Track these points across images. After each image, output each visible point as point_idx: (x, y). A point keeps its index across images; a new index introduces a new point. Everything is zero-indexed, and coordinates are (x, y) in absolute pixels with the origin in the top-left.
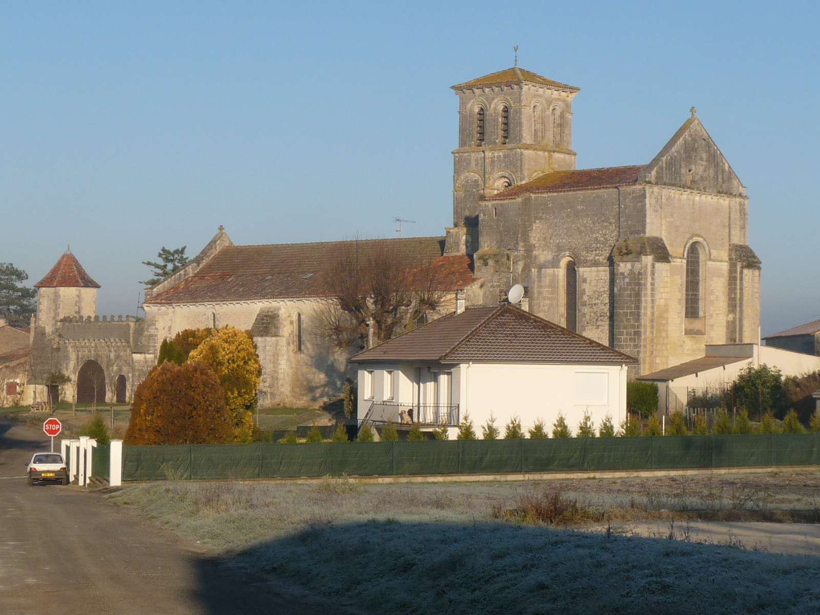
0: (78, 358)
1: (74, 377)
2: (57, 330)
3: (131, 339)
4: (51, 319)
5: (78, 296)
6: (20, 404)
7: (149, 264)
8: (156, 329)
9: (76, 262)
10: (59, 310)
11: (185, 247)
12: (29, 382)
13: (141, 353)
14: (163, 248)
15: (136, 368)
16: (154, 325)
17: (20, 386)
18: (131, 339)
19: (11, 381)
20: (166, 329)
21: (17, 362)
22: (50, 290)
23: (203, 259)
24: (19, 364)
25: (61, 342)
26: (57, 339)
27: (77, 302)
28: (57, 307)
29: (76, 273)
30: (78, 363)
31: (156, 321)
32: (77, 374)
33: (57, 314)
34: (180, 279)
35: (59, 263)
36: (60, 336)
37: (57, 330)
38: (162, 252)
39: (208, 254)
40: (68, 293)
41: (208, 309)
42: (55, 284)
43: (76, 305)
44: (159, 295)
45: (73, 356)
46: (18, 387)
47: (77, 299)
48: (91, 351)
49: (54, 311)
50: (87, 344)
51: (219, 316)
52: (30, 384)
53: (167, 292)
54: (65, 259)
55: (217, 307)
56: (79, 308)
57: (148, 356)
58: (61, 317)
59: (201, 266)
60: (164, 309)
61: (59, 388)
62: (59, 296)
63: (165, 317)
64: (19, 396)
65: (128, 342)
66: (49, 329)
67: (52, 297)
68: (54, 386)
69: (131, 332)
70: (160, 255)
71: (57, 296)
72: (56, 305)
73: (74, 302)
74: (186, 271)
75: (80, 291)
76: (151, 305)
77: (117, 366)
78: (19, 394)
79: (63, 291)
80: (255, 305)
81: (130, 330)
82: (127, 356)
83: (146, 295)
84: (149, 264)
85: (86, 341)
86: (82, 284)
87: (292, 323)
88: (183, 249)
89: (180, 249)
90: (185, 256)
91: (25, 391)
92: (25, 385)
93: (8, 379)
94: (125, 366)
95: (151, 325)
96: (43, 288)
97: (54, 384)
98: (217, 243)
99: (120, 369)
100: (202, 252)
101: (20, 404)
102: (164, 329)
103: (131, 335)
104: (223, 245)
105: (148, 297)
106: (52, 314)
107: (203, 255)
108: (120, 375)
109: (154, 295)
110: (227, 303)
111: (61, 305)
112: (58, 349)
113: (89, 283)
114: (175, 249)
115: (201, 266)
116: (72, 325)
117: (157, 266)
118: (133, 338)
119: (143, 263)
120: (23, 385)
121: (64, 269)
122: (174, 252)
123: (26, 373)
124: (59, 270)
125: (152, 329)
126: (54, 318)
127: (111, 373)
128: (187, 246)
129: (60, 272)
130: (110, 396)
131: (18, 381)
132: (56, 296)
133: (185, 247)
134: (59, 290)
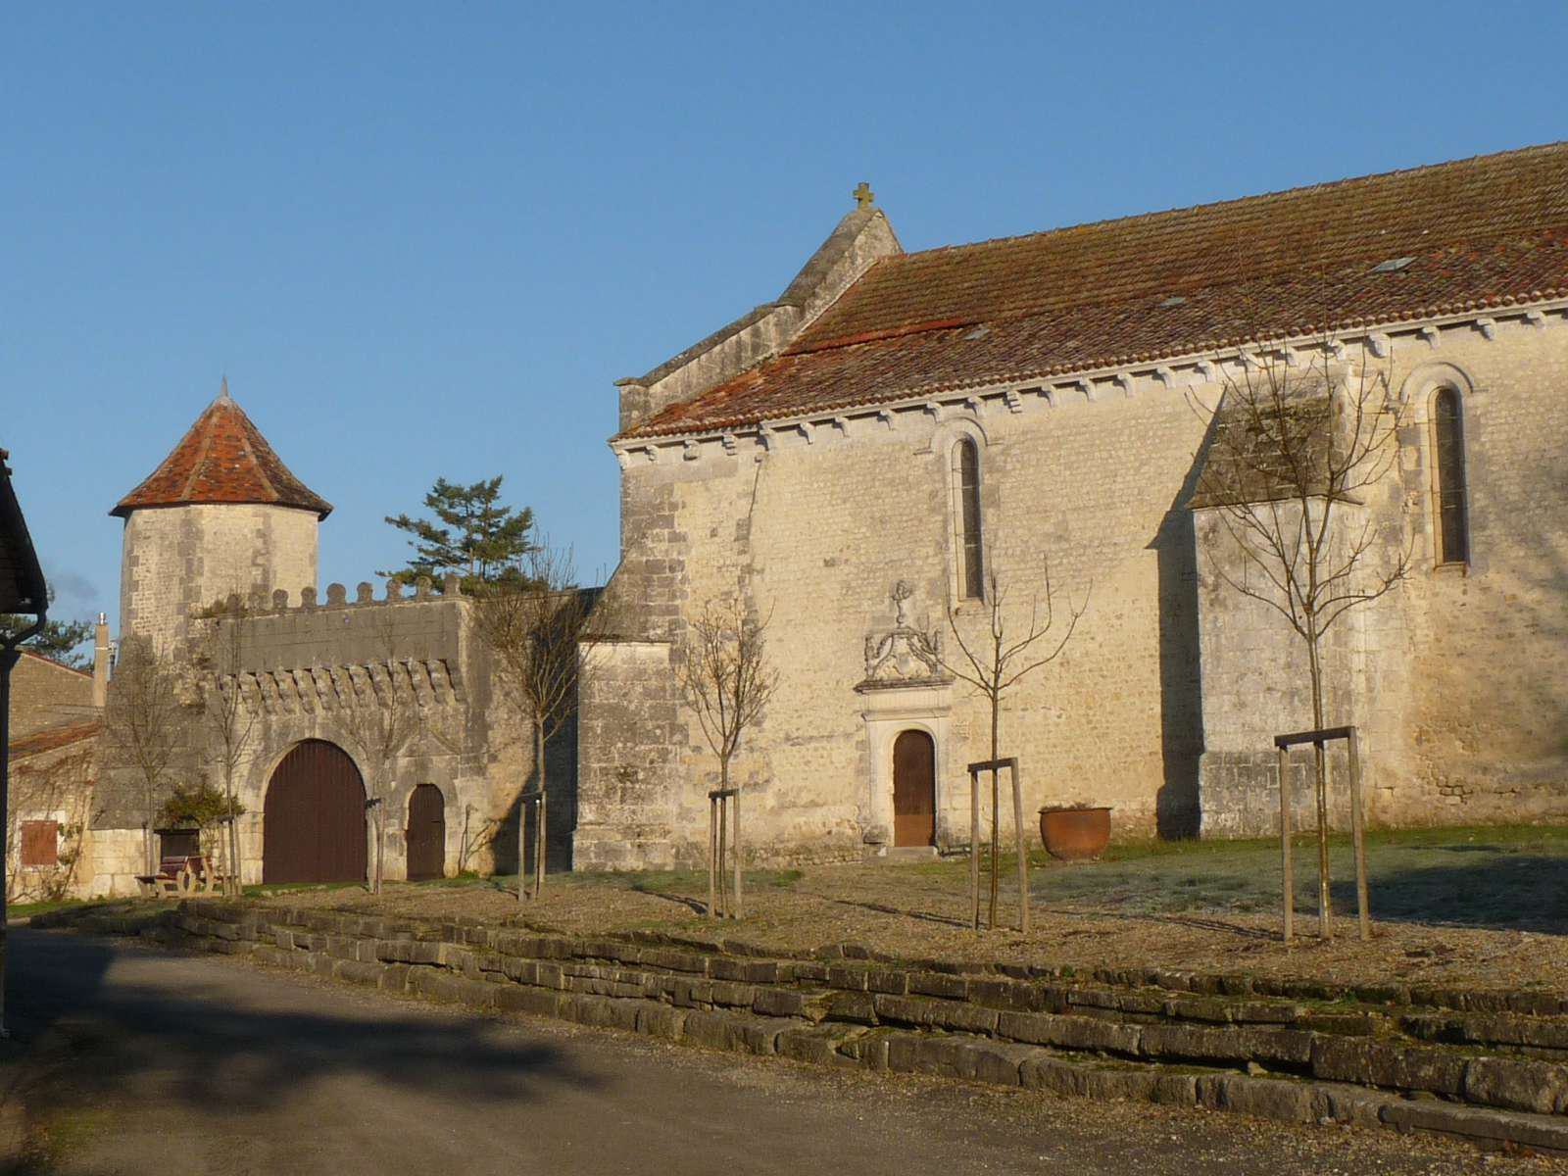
0: (266, 735)
1: (253, 801)
2: (192, 644)
3: (463, 658)
4: (171, 609)
5: (262, 534)
6: (68, 896)
7: (403, 523)
8: (676, 538)
9: (249, 429)
10: (201, 581)
11: (499, 480)
12: (100, 821)
13: (616, 638)
14: (441, 481)
15: (597, 701)
16: (669, 522)
17: (70, 835)
18: (463, 658)
19: (40, 816)
20: (728, 531)
21: (58, 753)
22: (168, 518)
23: (814, 295)
24: (62, 762)
25: (206, 686)
26: (191, 676)
27: (257, 553)
28: (191, 570)
29: (254, 460)
30: (267, 749)
31: (674, 507)
32: (265, 786)
33: (190, 594)
34: (739, 359)
35: (198, 433)
36: (203, 663)
37: (192, 644)
38: (435, 495)
39: (830, 278)
40: (228, 525)
41: (942, 424)
42: (186, 495)
43: (254, 564)
44: (671, 411)
45: (245, 722)
46: (60, 839)
47: (259, 543)
48: (312, 710)
49: (182, 580)
50: (302, 685)
51: (994, 449)
52: (102, 827)
53: (706, 399)
54: (214, 420)
55: (991, 413)
56: (266, 573)
57: (642, 650)
58: (207, 601)
59: (811, 318)
60: (711, 451)
61: (202, 837)
62: (199, 535)
63: (718, 484)
64: (63, 869)
65: (449, 668)
66: (165, 643)
67: (177, 537)
68: (180, 832)
69: (463, 633)
70: (431, 502)
71: (191, 534)
72: (189, 563)
73: (250, 553)
74: (756, 334)
75: (267, 516)
76: (650, 443)
77: (411, 753)
78: (66, 861)
79: (214, 518)
80: (1196, 380)
81: (458, 625)
82: (444, 719)
83: (627, 405)
84: (403, 523)
85: (298, 673)
86: (275, 496)
87: (1405, 436)
88: (496, 483)
89: (487, 485)
90: (495, 505)
91: (85, 852)
92: (86, 833)
93: (29, 812)
94: (440, 753)
95: (652, 524)
96: (146, 512)
97: (184, 826)
98: (857, 242)
99: (422, 766)
100: (808, 270)
101: (68, 896)
102: (714, 534)
103: (463, 644)
104: (875, 253)
105: (635, 414)
106: (176, 594)
107: (810, 280)
108: (420, 786)
109: (656, 410)
110: (1046, 383)
111: (206, 562)
112: (198, 708)
113: (295, 497)
114: (474, 484)
115: (811, 318)
116: (238, 625)
117: (427, 533)
118: (469, 657)
119: (389, 520)
120: (80, 830)
121: (213, 449)
122: (472, 489)
123: (89, 792)
124: (196, 451)
125: (658, 539)
126: (181, 608)
127: (389, 780)
128: (504, 477)
129: (200, 459)
130: (389, 858)
131: (61, 817)
132: (188, 534)
133: (499, 480)
134: (201, 513)
